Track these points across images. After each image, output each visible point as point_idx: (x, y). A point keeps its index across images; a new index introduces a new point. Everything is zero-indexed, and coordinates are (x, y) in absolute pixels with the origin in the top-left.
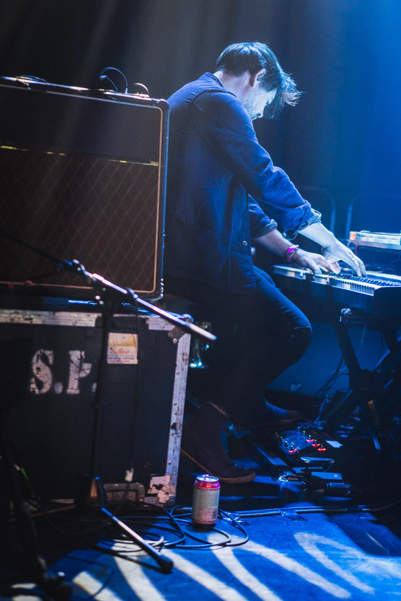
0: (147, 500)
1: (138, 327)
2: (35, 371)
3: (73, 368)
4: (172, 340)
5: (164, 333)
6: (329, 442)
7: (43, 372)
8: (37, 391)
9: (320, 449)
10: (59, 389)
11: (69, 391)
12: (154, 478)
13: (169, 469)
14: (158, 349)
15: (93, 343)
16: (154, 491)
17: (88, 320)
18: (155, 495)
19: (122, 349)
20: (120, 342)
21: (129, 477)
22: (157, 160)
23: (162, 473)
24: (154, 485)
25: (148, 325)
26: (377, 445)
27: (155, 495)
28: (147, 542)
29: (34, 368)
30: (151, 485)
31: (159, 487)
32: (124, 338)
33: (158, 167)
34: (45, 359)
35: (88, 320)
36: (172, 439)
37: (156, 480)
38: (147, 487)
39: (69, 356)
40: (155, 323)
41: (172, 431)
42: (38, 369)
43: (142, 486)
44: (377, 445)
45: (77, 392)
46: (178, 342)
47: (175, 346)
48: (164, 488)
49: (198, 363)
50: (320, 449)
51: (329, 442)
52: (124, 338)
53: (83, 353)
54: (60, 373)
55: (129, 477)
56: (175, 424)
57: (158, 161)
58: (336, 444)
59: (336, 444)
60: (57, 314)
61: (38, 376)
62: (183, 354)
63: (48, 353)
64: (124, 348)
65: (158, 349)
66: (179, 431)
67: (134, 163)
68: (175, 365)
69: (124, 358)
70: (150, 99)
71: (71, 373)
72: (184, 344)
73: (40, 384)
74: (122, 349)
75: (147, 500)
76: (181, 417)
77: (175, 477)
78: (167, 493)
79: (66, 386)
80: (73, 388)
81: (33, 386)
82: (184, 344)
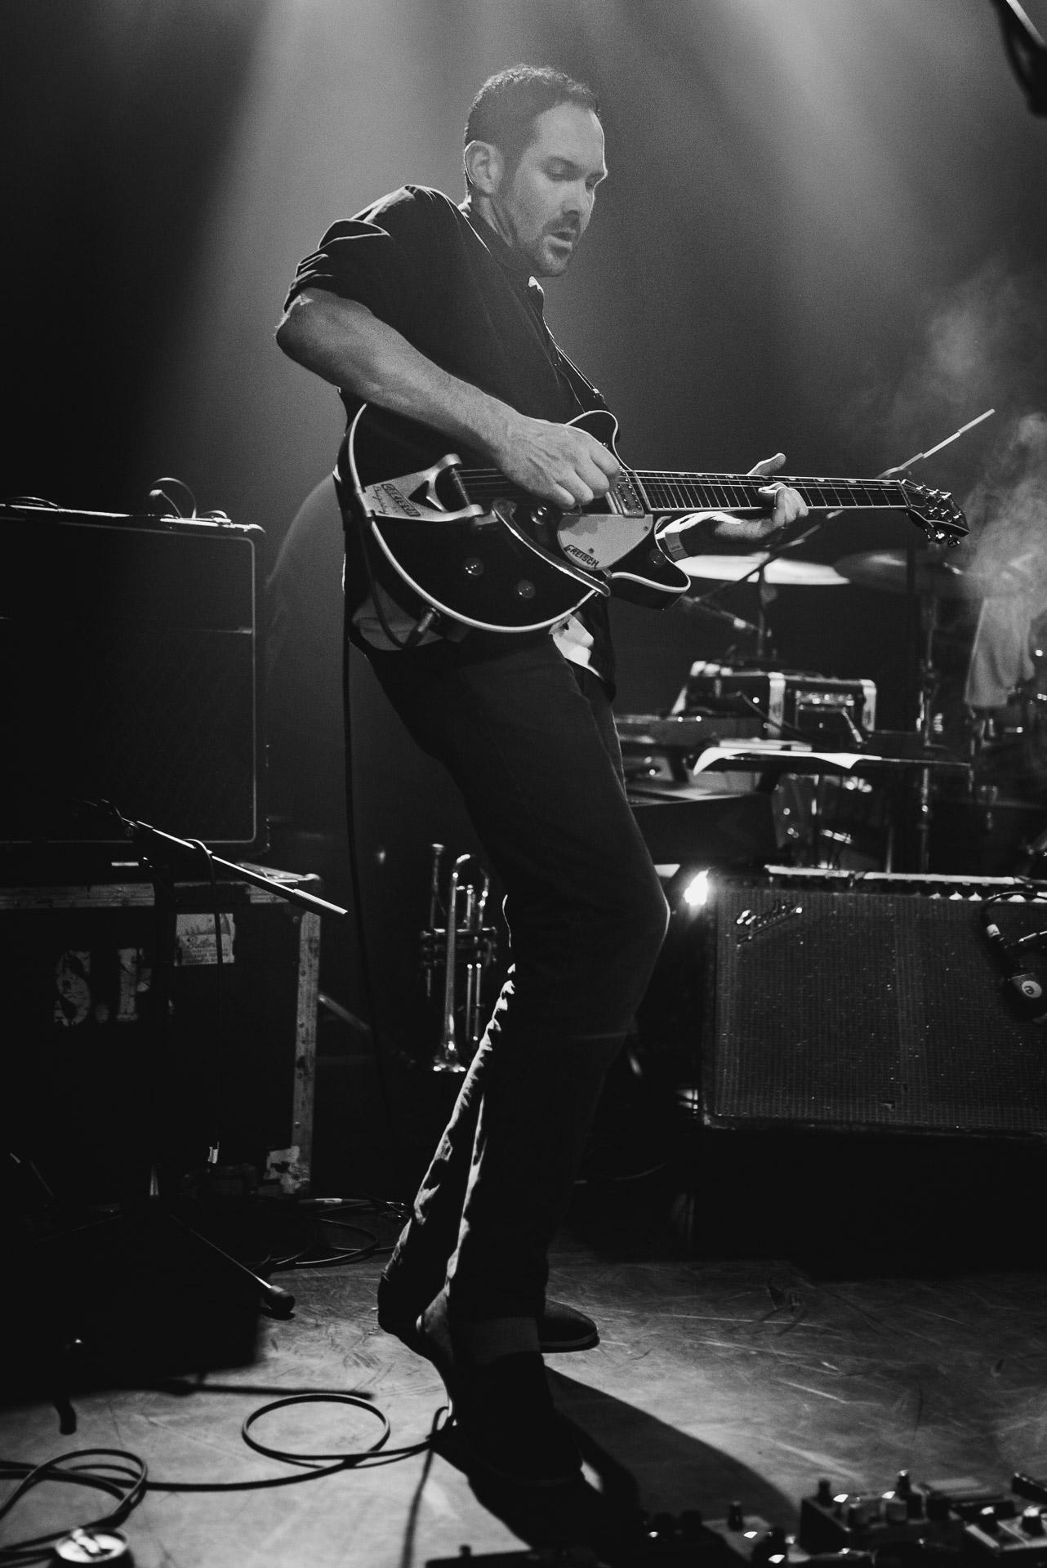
0: (262, 1191)
2: (61, 988)
3: (124, 978)
8: (65, 1022)
10: (103, 1016)
13: (297, 1135)
15: (154, 933)
16: (274, 1175)
17: (145, 895)
18: (277, 1181)
20: (203, 928)
22: (249, 626)
23: (286, 1144)
24: (273, 1165)
25: (248, 897)
26: (635, 1067)
27: (277, 1181)
28: (255, 1378)
29: (59, 983)
31: (283, 1167)
34: (77, 967)
36: (299, 1085)
37: (274, 1157)
38: (262, 1168)
39: (119, 958)
41: (298, 1071)
43: (252, 1168)
44: (635, 1067)
45: (134, 1017)
46: (300, 921)
48: (291, 1169)
49: (702, 672)
54: (105, 987)
56: (302, 1058)
60: (95, 889)
63: (80, 955)
64: (203, 935)
66: (311, 1070)
67: (307, 984)
68: (298, 960)
70: (233, 526)
71: (123, 986)
72: (310, 927)
73: (70, 1010)
75: (262, 1191)
76: (312, 1046)
77: (307, 1148)
78: (296, 1177)
79: (114, 1008)
80: (128, 1008)
81: (59, 1013)
82: (310, 927)
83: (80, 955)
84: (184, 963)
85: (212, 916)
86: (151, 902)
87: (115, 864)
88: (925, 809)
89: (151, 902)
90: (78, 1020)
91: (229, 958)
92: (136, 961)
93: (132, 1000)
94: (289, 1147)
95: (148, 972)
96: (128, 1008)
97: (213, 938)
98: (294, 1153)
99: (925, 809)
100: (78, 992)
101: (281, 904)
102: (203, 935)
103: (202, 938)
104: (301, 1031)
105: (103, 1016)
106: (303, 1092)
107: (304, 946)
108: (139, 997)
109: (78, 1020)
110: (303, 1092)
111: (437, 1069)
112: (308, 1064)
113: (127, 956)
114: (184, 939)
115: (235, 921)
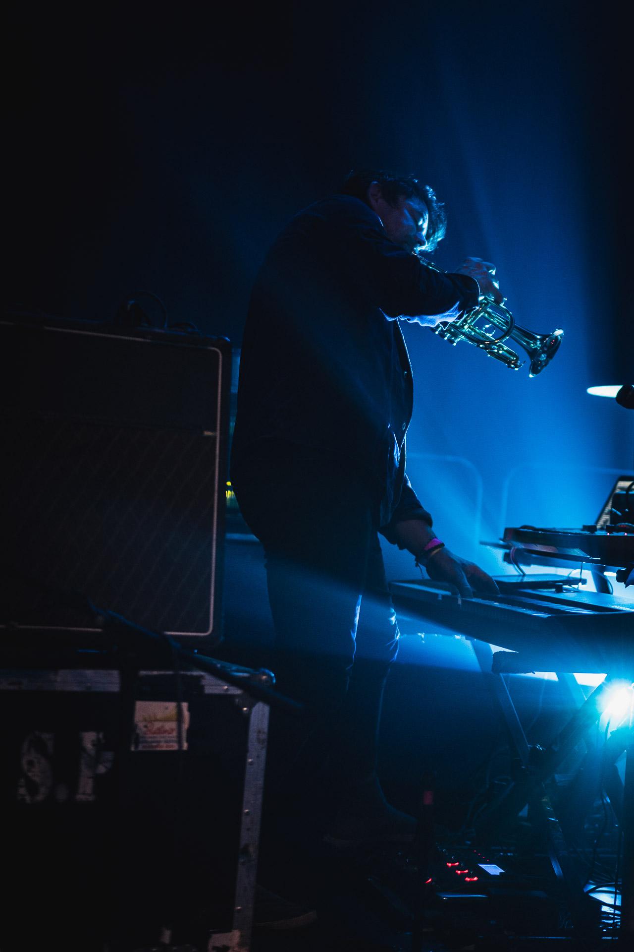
1: (189, 692)
2: (25, 767)
4: (241, 709)
5: (226, 698)
6: (483, 866)
7: (36, 768)
8: (28, 799)
9: (468, 879)
10: (62, 795)
11: (80, 797)
12: (214, 936)
14: (216, 725)
15: (115, 717)
17: (110, 681)
19: (163, 727)
21: (167, 936)
23: (227, 928)
25: (203, 687)
29: (24, 762)
30: (210, 947)
32: (167, 708)
33: (215, 437)
35: (110, 681)
40: (213, 686)
42: (31, 763)
47: (246, 719)
50: (468, 879)
51: (483, 866)
52: (167, 708)
53: (101, 735)
55: (167, 936)
56: (247, 846)
57: (214, 430)
58: (494, 870)
59: (494, 870)
61: (30, 774)
62: (259, 732)
63: (46, 736)
64: (161, 722)
65: (216, 725)
69: (166, 742)
73: (33, 788)
74: (163, 727)
80: (86, 788)
81: (22, 791)
83: (46, 736)
84: (140, 748)
85: (172, 706)
86: (115, 688)
87: (143, 673)
88: (476, 879)
89: (115, 688)
90: (39, 798)
91: (185, 746)
92: (97, 744)
93: (90, 781)
94: (229, 930)
95: (109, 755)
96: (86, 788)
97: (174, 725)
98: (236, 935)
99: (476, 879)
100: (36, 768)
101: (233, 696)
102: (161, 722)
103: (157, 725)
104: (245, 820)
105: (62, 795)
106: (245, 878)
107: (252, 735)
108: (98, 779)
109: (39, 798)
110: (245, 878)
111: (609, 801)
112: (251, 849)
113: (89, 739)
114: (141, 725)
115: (190, 710)
